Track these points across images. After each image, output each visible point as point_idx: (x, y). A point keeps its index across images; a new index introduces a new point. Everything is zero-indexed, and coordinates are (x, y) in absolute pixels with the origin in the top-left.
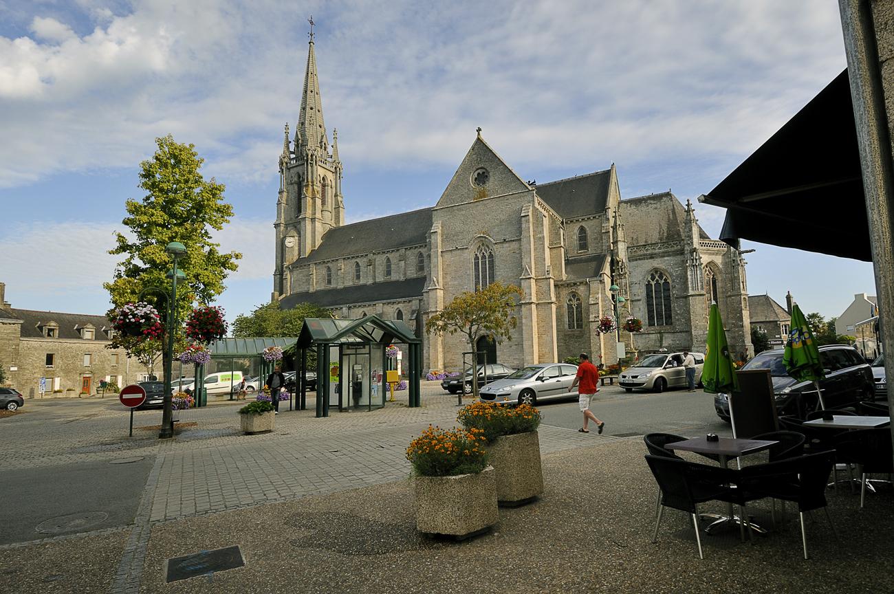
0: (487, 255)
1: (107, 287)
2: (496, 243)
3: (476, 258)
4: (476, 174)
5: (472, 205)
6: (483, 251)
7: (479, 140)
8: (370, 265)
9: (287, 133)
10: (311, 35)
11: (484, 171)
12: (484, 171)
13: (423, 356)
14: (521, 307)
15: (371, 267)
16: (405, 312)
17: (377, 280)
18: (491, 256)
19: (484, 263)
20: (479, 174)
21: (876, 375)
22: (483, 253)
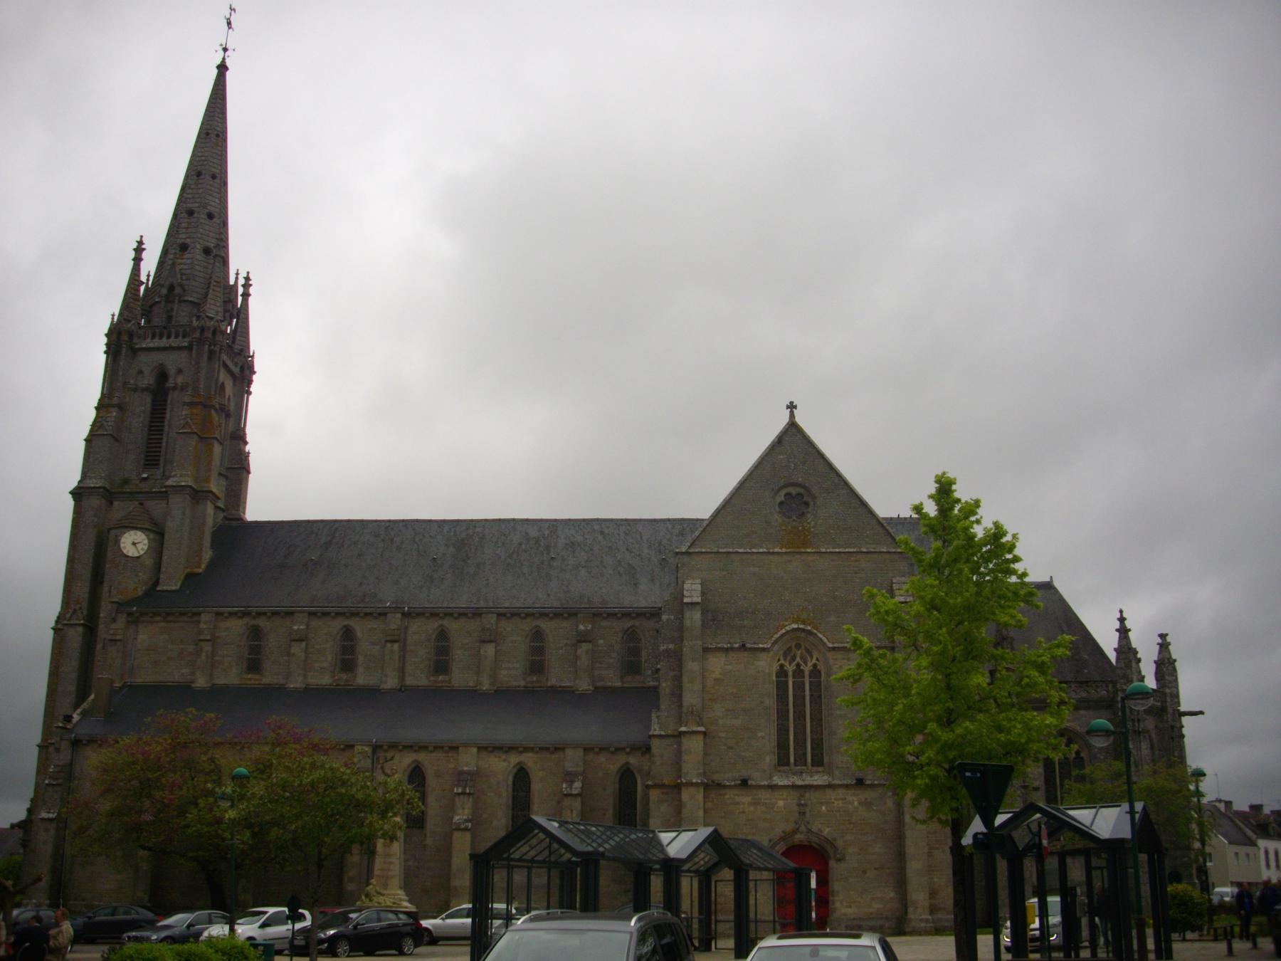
0: (807, 669)
1: (977, 503)
2: (834, 649)
3: (782, 672)
4: (782, 493)
5: (776, 558)
6: (798, 659)
7: (793, 428)
8: (393, 642)
9: (138, 260)
10: (225, 50)
11: (802, 491)
12: (802, 491)
13: (1023, 880)
14: (679, 793)
15: (396, 646)
16: (541, 774)
17: (409, 681)
18: (815, 672)
19: (799, 687)
20: (788, 494)
21: (462, 954)
22: (798, 665)
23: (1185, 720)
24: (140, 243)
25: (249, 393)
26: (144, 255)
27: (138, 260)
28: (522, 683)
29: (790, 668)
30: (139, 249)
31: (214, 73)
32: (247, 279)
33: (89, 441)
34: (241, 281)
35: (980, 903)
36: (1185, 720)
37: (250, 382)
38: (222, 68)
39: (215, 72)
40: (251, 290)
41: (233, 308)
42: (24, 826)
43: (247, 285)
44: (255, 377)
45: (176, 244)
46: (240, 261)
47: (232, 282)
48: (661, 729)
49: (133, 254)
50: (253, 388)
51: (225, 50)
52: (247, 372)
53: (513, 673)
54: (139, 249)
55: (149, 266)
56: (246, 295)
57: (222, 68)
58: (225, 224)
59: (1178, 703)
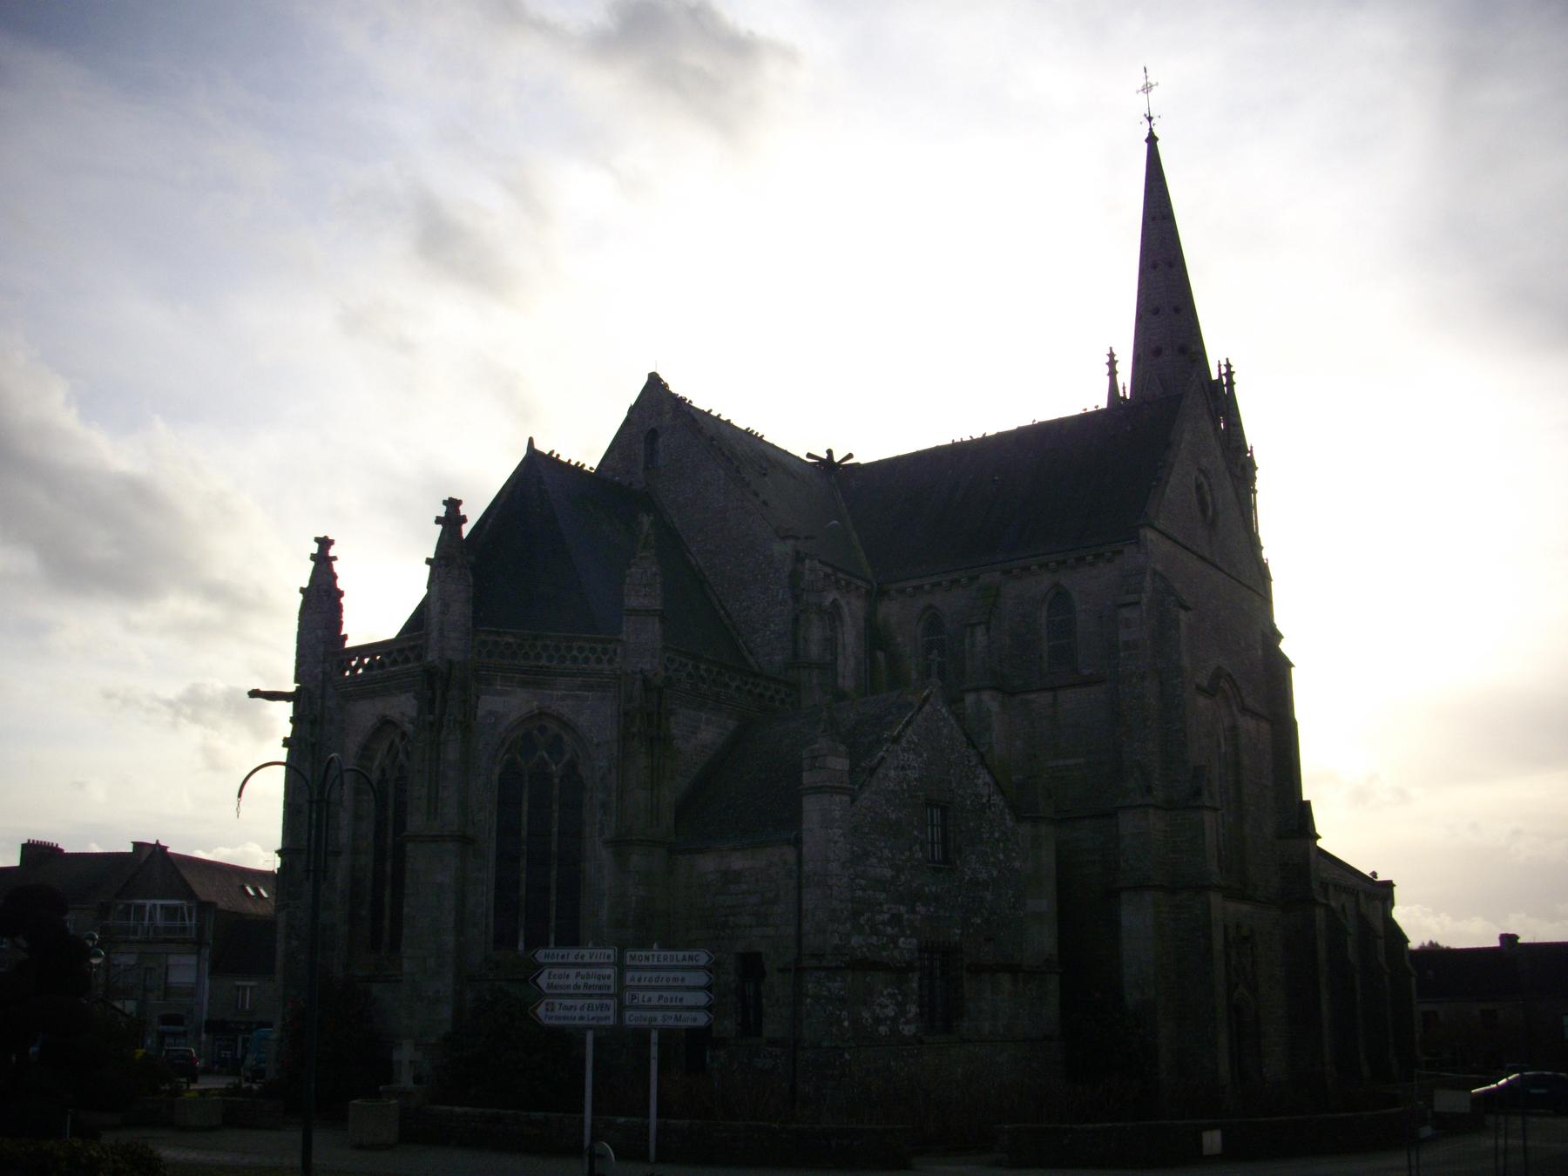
9: (1113, 374)
10: (1150, 119)
23: (291, 687)
24: (1112, 355)
25: (1255, 492)
26: (1118, 367)
27: (1113, 374)
28: (172, 960)
30: (1112, 363)
31: (1144, 148)
32: (1228, 366)
34: (1224, 370)
36: (291, 687)
37: (1254, 479)
38: (1152, 140)
40: (1235, 378)
41: (1219, 400)
43: (1229, 374)
44: (1257, 473)
46: (1216, 353)
47: (1215, 376)
49: (1107, 370)
50: (1258, 485)
51: (1150, 119)
53: (168, 1040)
54: (1112, 363)
56: (1231, 384)
57: (1152, 140)
59: (1405, 940)
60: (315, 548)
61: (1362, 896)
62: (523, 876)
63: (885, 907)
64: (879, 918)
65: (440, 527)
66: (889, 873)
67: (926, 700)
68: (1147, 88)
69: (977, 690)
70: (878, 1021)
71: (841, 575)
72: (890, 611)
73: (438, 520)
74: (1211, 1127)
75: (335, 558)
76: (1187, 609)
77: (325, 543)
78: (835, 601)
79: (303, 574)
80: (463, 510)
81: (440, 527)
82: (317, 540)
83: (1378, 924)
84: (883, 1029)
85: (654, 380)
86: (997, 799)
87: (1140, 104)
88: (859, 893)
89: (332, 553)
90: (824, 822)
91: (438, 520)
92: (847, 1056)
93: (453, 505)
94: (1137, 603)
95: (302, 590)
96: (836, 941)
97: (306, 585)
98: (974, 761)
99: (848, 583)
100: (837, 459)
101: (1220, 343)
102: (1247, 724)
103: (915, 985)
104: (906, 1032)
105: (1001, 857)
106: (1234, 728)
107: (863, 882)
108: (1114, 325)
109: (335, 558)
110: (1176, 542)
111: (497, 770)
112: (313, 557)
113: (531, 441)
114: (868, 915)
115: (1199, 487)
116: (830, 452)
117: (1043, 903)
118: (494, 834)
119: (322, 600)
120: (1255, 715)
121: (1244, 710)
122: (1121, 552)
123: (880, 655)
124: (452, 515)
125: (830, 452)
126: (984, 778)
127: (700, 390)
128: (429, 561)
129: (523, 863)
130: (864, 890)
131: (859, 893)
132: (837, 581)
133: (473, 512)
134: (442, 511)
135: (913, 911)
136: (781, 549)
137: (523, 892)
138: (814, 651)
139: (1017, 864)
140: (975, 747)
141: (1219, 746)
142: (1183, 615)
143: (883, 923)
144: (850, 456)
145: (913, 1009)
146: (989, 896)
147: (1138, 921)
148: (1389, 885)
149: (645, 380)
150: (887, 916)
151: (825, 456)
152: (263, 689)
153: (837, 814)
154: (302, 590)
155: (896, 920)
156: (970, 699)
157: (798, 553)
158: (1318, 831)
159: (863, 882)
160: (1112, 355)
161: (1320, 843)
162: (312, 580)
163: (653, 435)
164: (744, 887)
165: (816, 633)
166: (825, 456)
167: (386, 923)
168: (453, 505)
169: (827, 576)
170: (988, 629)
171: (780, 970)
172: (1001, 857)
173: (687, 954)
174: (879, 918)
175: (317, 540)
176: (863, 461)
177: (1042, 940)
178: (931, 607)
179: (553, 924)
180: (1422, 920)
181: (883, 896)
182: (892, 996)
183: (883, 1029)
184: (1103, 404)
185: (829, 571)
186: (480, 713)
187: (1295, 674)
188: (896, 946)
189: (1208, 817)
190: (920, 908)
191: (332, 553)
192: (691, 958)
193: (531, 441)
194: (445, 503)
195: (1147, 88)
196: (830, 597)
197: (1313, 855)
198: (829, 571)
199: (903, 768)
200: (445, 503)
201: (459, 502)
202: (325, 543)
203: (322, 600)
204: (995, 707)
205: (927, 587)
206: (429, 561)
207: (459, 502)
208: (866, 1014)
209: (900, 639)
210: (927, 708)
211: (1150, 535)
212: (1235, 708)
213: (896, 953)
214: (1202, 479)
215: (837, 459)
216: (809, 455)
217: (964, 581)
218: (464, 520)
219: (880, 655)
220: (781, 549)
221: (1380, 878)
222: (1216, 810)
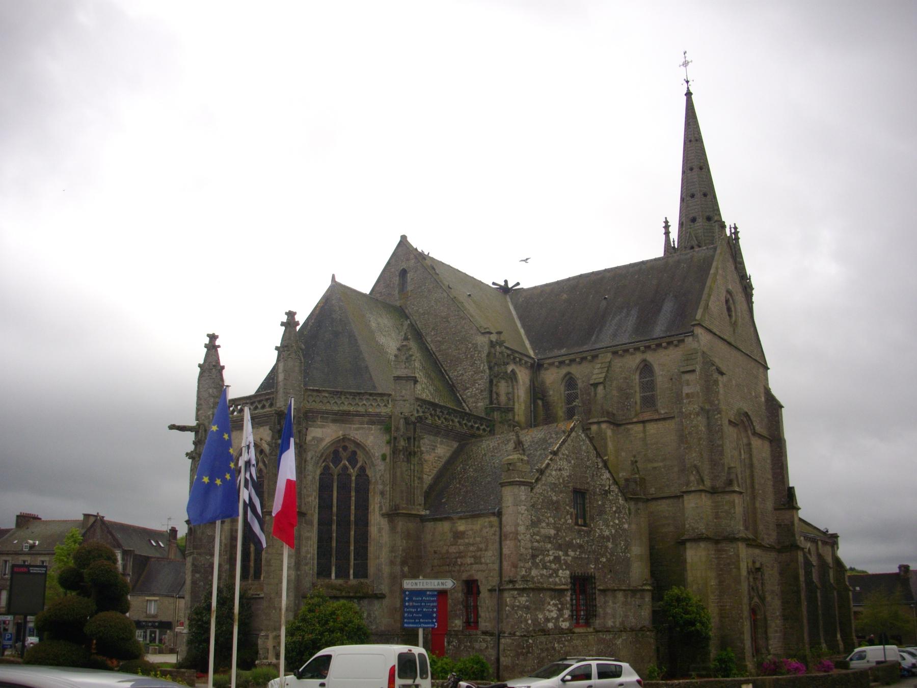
9: (667, 233)
10: (687, 82)
22: (345, 468)
24: (666, 222)
26: (670, 229)
27: (667, 233)
29: (335, 470)
30: (667, 226)
32: (735, 228)
33: (199, 380)
34: (733, 231)
35: (252, 571)
36: (193, 423)
38: (689, 94)
39: (685, 98)
40: (739, 235)
42: (293, 526)
43: (736, 233)
44: (754, 292)
45: (687, 219)
48: (733, 504)
49: (663, 231)
51: (687, 82)
52: (749, 290)
54: (667, 226)
55: (674, 235)
56: (737, 239)
57: (689, 94)
58: (715, 197)
60: (207, 340)
61: (820, 543)
62: (334, 535)
63: (551, 553)
64: (547, 559)
65: (283, 328)
66: (552, 532)
67: (572, 429)
68: (686, 64)
69: (599, 423)
70: (547, 620)
71: (517, 355)
72: (552, 377)
73: (283, 324)
74: (401, 584)
75: (219, 346)
76: (722, 374)
77: (213, 337)
78: (513, 371)
79: (200, 355)
80: (297, 318)
81: (283, 328)
82: (208, 335)
83: (829, 560)
84: (550, 625)
85: (404, 238)
86: (614, 488)
87: (682, 73)
88: (536, 544)
89: (217, 343)
90: (516, 506)
91: (283, 324)
92: (530, 641)
93: (291, 315)
94: (693, 371)
95: (200, 366)
96: (524, 573)
97: (202, 362)
98: (601, 465)
99: (520, 360)
100: (510, 286)
101: (730, 212)
102: (756, 443)
103: (568, 599)
104: (563, 627)
105: (617, 522)
106: (749, 444)
107: (538, 538)
108: (668, 204)
109: (219, 346)
110: (715, 334)
111: (318, 472)
112: (206, 346)
113: (333, 277)
114: (540, 557)
115: (727, 301)
116: (506, 282)
117: (638, 550)
118: (317, 511)
119: (211, 369)
120: (760, 436)
121: (755, 434)
122: (683, 341)
123: (540, 402)
124: (290, 322)
125: (506, 282)
126: (606, 475)
127: (419, 243)
128: (277, 348)
129: (334, 527)
130: (538, 541)
131: (536, 544)
132: (514, 358)
133: (301, 318)
134: (285, 319)
135: (567, 555)
136: (482, 340)
137: (334, 544)
138: (503, 398)
139: (626, 526)
140: (601, 457)
141: (740, 455)
142: (720, 378)
143: (550, 562)
144: (518, 284)
145: (567, 613)
146: (610, 545)
147: (696, 557)
148: (835, 537)
149: (399, 239)
150: (552, 558)
151: (503, 284)
152: (177, 424)
153: (523, 498)
154: (200, 366)
155: (557, 559)
156: (594, 428)
157: (492, 342)
158: (800, 504)
159: (538, 538)
160: (666, 222)
161: (801, 514)
162: (205, 360)
163: (404, 273)
164: (467, 541)
165: (502, 387)
166: (503, 284)
167: (252, 564)
168: (291, 315)
169: (508, 355)
170: (605, 387)
171: (490, 590)
172: (617, 522)
173: (440, 581)
174: (547, 559)
175: (208, 335)
176: (525, 287)
177: (638, 571)
178: (569, 373)
179: (352, 563)
180: (854, 554)
181: (550, 545)
182: (555, 605)
183: (550, 625)
184: (659, 252)
185: (509, 352)
186: (309, 438)
187: (785, 412)
188: (557, 576)
189: (737, 499)
190: (571, 553)
191: (217, 343)
192: (443, 584)
193: (333, 277)
194: (286, 313)
195: (686, 64)
196: (510, 368)
197: (796, 521)
198: (509, 352)
199: (560, 470)
200: (286, 313)
201: (295, 313)
202: (213, 337)
203: (211, 369)
204: (609, 433)
205: (567, 362)
206: (277, 348)
207: (295, 313)
208: (540, 616)
209: (551, 393)
210: (573, 434)
211: (699, 331)
212: (749, 432)
213: (557, 580)
214: (728, 296)
215: (510, 286)
216: (494, 284)
217: (589, 358)
218: (298, 324)
219: (540, 402)
220: (482, 340)
221: (830, 532)
222: (741, 493)
